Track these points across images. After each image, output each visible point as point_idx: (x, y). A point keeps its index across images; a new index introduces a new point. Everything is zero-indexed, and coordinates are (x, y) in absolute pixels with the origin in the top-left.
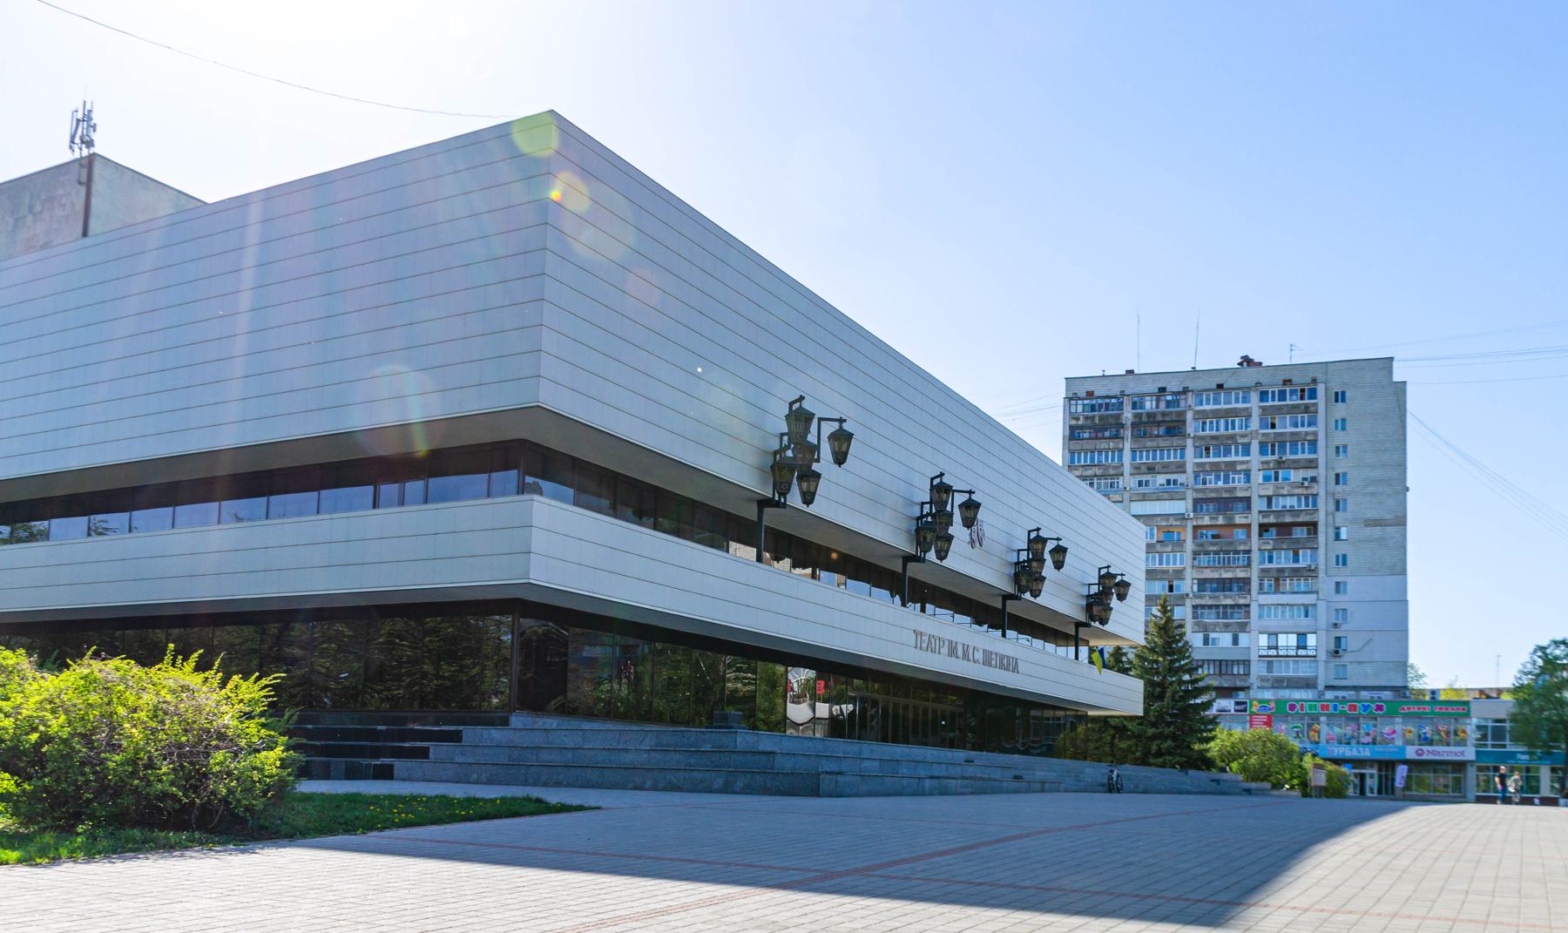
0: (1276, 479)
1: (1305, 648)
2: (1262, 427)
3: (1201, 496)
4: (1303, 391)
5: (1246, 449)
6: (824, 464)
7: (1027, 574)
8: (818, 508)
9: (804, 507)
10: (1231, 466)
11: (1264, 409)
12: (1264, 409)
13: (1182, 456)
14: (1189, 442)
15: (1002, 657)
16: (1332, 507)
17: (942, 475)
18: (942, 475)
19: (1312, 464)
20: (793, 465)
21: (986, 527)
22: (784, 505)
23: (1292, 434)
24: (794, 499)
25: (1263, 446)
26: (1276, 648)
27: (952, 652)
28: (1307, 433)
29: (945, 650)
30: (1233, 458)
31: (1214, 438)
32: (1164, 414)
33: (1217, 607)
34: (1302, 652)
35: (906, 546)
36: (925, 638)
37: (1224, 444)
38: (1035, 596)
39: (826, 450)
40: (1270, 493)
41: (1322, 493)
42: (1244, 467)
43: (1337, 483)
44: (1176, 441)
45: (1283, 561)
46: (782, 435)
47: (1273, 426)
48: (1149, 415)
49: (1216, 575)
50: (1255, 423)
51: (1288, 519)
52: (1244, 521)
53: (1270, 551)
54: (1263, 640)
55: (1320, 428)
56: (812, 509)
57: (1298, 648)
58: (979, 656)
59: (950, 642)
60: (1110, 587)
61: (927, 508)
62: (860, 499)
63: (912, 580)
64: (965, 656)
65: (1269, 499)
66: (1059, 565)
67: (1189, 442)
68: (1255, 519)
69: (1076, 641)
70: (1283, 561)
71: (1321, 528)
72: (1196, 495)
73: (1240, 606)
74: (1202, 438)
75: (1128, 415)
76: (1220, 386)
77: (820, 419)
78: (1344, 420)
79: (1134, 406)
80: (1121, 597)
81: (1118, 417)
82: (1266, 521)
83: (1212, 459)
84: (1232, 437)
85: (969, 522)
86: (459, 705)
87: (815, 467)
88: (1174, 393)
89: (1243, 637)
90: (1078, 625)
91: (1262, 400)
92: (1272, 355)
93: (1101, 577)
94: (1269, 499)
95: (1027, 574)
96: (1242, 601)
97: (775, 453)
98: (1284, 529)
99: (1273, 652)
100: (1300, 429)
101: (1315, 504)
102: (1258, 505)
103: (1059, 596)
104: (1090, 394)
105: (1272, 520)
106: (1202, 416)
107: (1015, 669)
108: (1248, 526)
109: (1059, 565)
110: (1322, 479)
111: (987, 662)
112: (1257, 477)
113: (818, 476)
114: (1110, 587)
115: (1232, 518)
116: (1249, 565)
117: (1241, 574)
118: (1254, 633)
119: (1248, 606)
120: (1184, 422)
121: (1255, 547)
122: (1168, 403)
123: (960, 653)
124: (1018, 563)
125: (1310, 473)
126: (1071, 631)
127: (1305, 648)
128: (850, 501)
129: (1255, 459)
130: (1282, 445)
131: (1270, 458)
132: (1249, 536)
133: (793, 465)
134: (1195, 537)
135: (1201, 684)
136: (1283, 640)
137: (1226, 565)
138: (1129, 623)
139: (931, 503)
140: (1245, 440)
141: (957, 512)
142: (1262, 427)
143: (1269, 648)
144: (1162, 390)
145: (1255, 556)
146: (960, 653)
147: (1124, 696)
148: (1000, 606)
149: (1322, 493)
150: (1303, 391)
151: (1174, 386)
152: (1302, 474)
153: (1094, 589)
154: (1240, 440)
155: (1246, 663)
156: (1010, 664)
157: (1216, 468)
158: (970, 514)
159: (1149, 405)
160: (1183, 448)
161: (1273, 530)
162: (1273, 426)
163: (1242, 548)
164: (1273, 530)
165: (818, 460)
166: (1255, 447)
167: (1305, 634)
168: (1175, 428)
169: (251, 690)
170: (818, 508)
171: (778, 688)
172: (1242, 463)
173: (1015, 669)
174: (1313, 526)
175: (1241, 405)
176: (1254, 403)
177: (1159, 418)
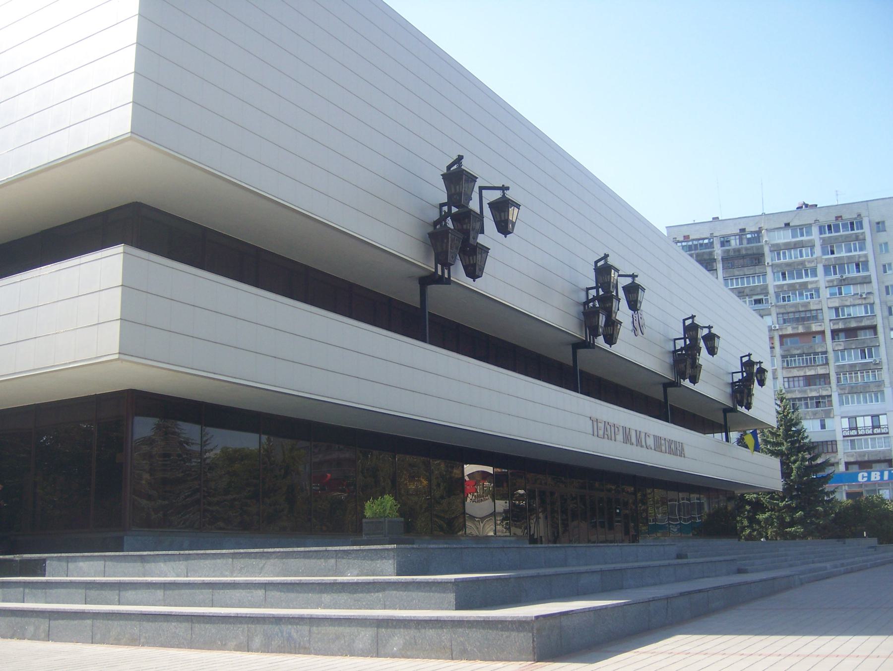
0: (840, 293)
1: (879, 427)
2: (824, 253)
3: (782, 311)
4: (852, 224)
5: (814, 273)
6: (489, 236)
7: (685, 361)
9: (606, 347)
10: (805, 284)
11: (824, 239)
12: (824, 239)
13: (764, 280)
14: (769, 270)
15: (670, 442)
16: (886, 313)
17: (606, 256)
19: (867, 281)
21: (644, 313)
22: (448, 281)
23: (849, 257)
25: (827, 268)
26: (856, 429)
27: (627, 439)
28: (859, 256)
29: (620, 437)
30: (805, 280)
31: (788, 265)
32: (746, 249)
33: (806, 399)
34: (876, 431)
36: (601, 425)
37: (797, 269)
40: (837, 305)
41: (877, 301)
42: (814, 286)
43: (888, 293)
44: (758, 269)
45: (853, 358)
46: (588, 289)
47: (832, 253)
48: (735, 250)
49: (802, 373)
50: (818, 251)
51: (853, 324)
52: (819, 329)
53: (842, 351)
54: (845, 423)
55: (869, 251)
57: (873, 427)
58: (651, 442)
59: (624, 428)
60: (752, 373)
61: (593, 293)
62: (525, 275)
64: (639, 443)
65: (837, 309)
66: (504, 227)
67: (769, 270)
68: (828, 327)
69: (725, 429)
70: (853, 358)
71: (880, 329)
72: (778, 310)
73: (823, 397)
74: (778, 265)
75: (718, 252)
76: (787, 225)
77: (481, 189)
78: (886, 244)
79: (723, 244)
80: (762, 383)
81: (711, 253)
82: (836, 327)
83: (788, 281)
84: (802, 263)
85: (634, 305)
88: (751, 233)
89: (828, 422)
90: (727, 410)
91: (821, 233)
92: (825, 197)
93: (743, 364)
94: (837, 309)
95: (685, 361)
96: (824, 393)
98: (850, 332)
99: (854, 432)
100: (853, 253)
101: (872, 311)
102: (828, 315)
103: (712, 382)
104: (686, 238)
105: (841, 326)
106: (777, 249)
107: (682, 454)
108: (823, 333)
109: (712, 351)
110: (876, 292)
111: (658, 447)
112: (825, 293)
114: (752, 373)
115: (809, 327)
116: (827, 364)
117: (821, 371)
118: (837, 418)
119: (830, 396)
120: (763, 255)
121: (830, 349)
122: (749, 241)
123: (634, 440)
124: (675, 351)
125: (866, 289)
126: (719, 418)
127: (879, 427)
129: (821, 279)
130: (842, 266)
131: (833, 277)
132: (824, 339)
134: (782, 344)
135: (819, 461)
136: (860, 422)
137: (812, 364)
138: (764, 406)
139: (597, 288)
140: (813, 265)
142: (824, 253)
143: (851, 429)
144: (743, 230)
145: (831, 355)
146: (634, 440)
147: (762, 472)
148: (661, 397)
149: (877, 301)
150: (852, 224)
151: (751, 228)
152: (859, 289)
153: (738, 377)
154: (808, 265)
155: (834, 443)
156: (676, 449)
157: (792, 287)
159: (734, 243)
160: (765, 275)
161: (842, 335)
162: (832, 253)
163: (820, 350)
164: (842, 335)
166: (820, 270)
167: (878, 416)
168: (757, 258)
171: (457, 487)
172: (812, 283)
173: (682, 454)
174: (874, 328)
175: (805, 238)
176: (815, 235)
177: (744, 252)
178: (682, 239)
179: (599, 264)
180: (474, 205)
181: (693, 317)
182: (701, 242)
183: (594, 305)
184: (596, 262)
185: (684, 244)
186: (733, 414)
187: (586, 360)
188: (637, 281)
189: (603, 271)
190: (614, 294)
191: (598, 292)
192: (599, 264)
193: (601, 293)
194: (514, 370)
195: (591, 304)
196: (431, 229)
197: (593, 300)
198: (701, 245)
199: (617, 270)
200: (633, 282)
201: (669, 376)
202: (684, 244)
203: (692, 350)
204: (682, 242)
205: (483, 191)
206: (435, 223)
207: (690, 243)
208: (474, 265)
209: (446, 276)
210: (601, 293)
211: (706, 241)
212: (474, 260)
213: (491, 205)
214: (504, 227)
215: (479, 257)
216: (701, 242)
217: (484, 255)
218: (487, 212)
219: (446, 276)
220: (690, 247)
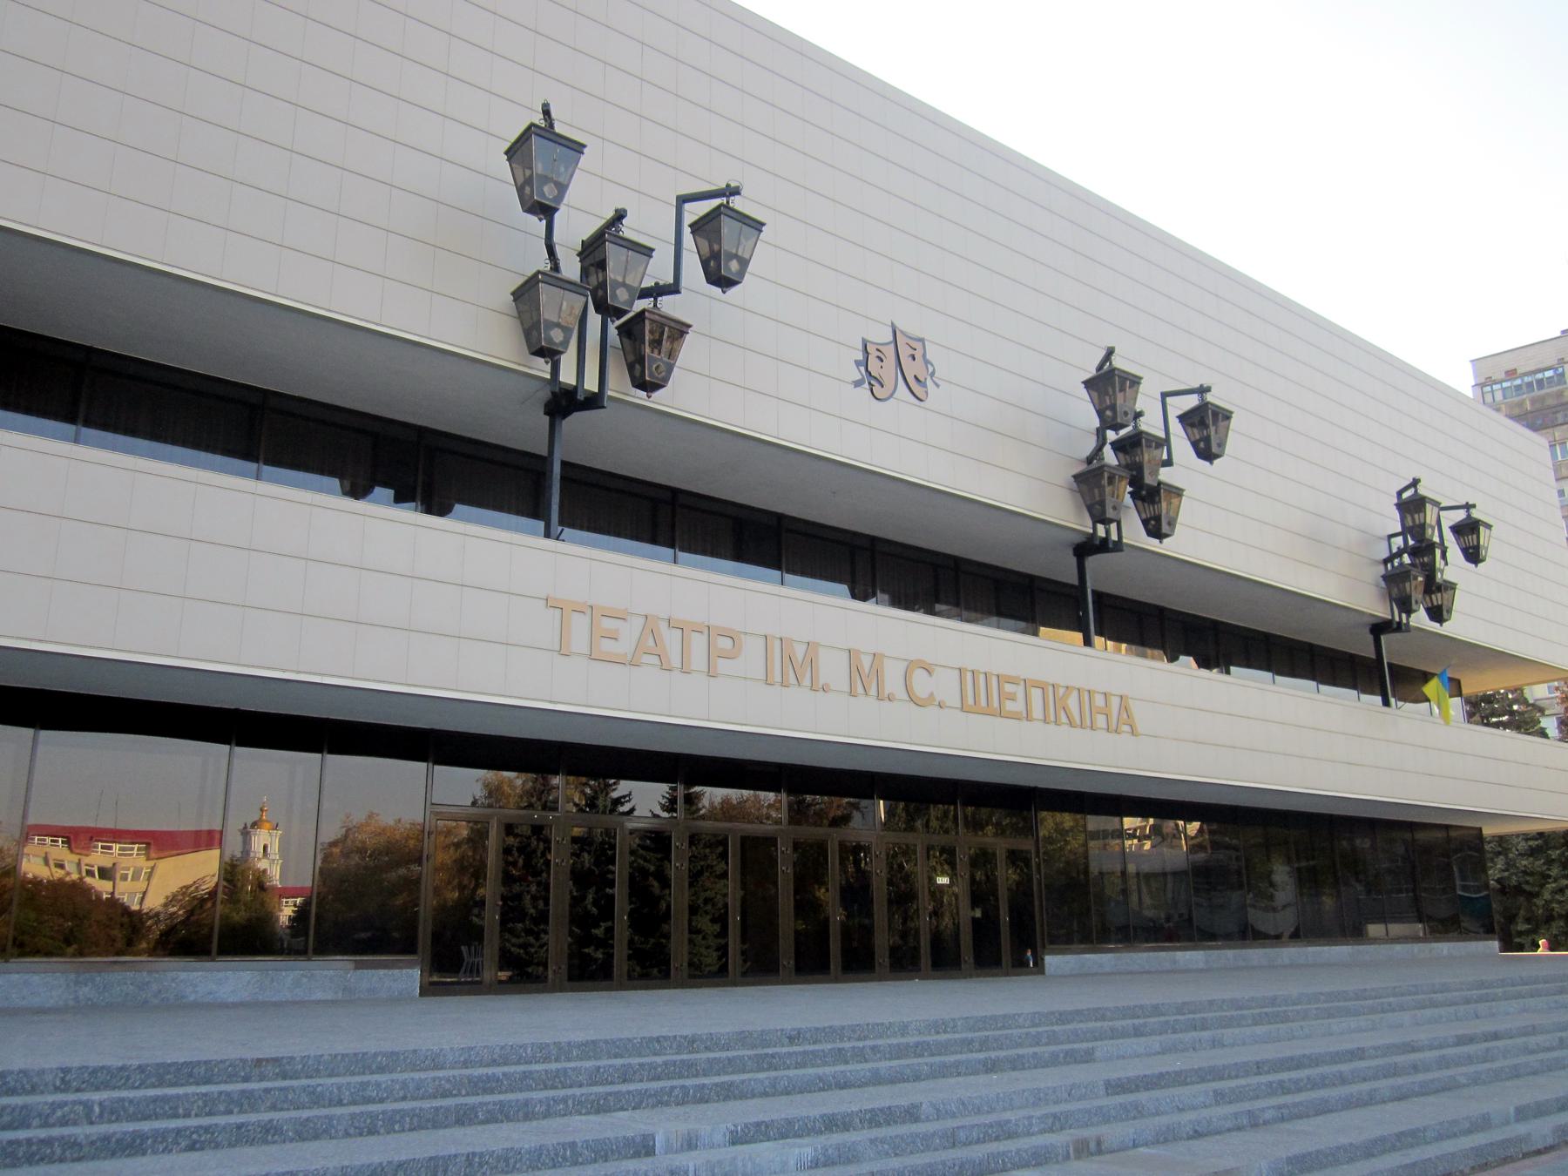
8: (1182, 544)
9: (1434, 627)
18: (1415, 483)
20: (1124, 471)
22: (1118, 546)
24: (1133, 531)
35: (1070, 516)
38: (650, 387)
39: (1181, 445)
46: (1391, 536)
56: (1447, 629)
61: (1398, 542)
63: (1098, 595)
66: (1473, 555)
86: (129, 946)
87: (1165, 475)
97: (1386, 561)
113: (1451, 587)
128: (1221, 528)
133: (1124, 471)
141: (1450, 539)
158: (1471, 539)
165: (1169, 463)
169: (821, 893)
170: (1182, 544)
178: (1503, 376)
179: (1405, 495)
180: (1151, 424)
181: (1415, 483)
182: (1539, 376)
183: (1401, 564)
184: (1400, 493)
185: (1505, 385)
186: (1397, 636)
187: (1102, 573)
188: (1475, 514)
189: (1412, 505)
190: (1436, 539)
191: (1405, 541)
192: (1405, 495)
193: (1411, 542)
194: (618, 535)
195: (1396, 562)
196: (1082, 468)
197: (1399, 554)
198: (1540, 383)
199: (1436, 504)
200: (1469, 516)
201: (1381, 610)
202: (1505, 385)
203: (1423, 550)
204: (1501, 382)
205: (1169, 400)
206: (1089, 460)
207: (1518, 382)
208: (1158, 519)
209: (1114, 537)
210: (1411, 542)
211: (1549, 374)
212: (1155, 504)
213: (1184, 418)
214: (1473, 555)
215: (1164, 505)
216: (1539, 376)
217: (1175, 501)
218: (1176, 428)
219: (1114, 537)
220: (1518, 388)
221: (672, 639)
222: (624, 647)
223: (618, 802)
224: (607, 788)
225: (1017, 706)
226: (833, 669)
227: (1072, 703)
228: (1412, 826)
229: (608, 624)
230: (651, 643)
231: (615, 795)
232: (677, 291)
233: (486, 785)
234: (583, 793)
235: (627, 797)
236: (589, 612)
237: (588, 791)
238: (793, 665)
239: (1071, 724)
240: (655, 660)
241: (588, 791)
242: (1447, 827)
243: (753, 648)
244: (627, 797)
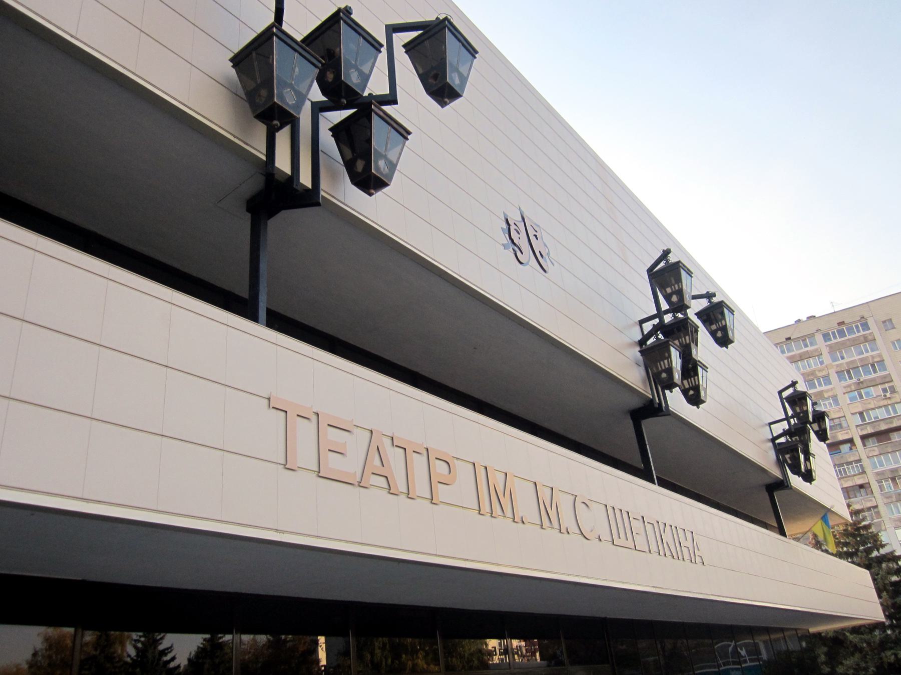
38: (369, 182)
200: (795, 390)
214: (724, 340)
221: (394, 457)
222: (350, 465)
223: (164, 652)
224: (157, 642)
225: (350, 465)
226: (594, 520)
227: (667, 537)
228: (732, 631)
229: (333, 435)
230: (377, 462)
231: (161, 647)
232: (395, 102)
233: (47, 639)
234: (135, 647)
235: (169, 649)
236: (314, 418)
237: (140, 645)
238: (675, 546)
239: (390, 490)
240: (382, 482)
241: (140, 645)
242: (796, 630)
243: (464, 472)
244: (169, 649)
